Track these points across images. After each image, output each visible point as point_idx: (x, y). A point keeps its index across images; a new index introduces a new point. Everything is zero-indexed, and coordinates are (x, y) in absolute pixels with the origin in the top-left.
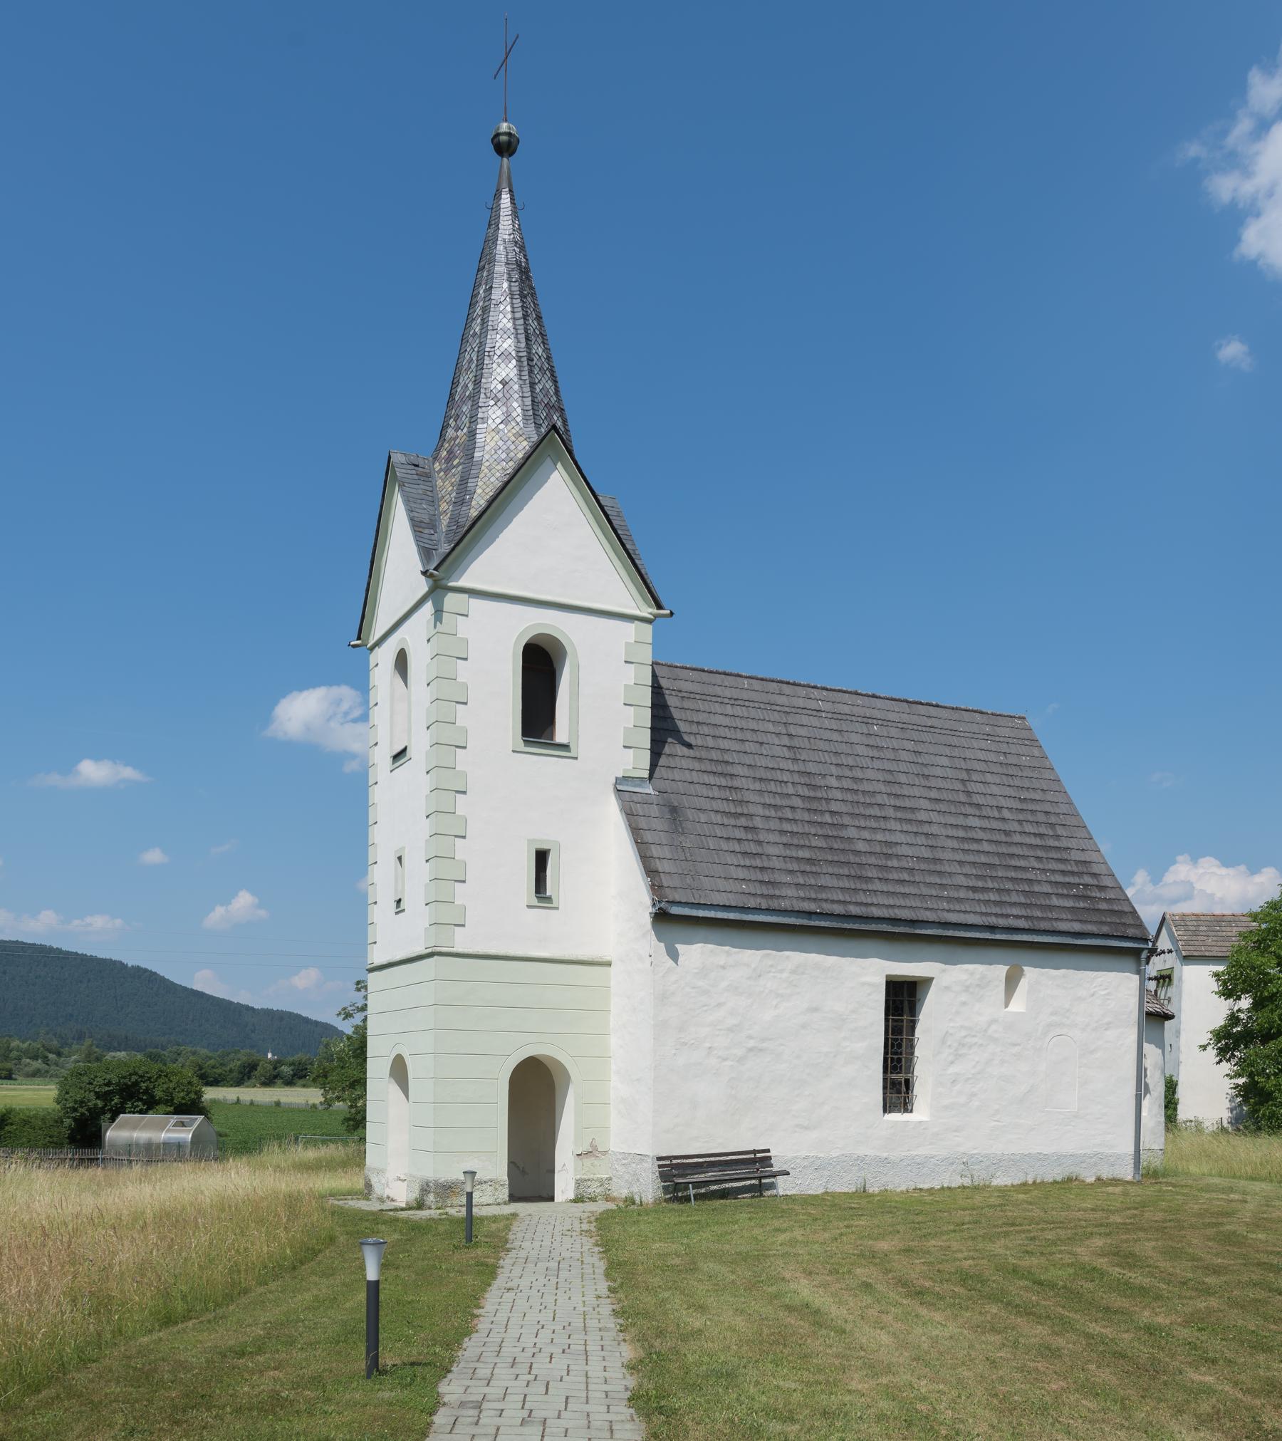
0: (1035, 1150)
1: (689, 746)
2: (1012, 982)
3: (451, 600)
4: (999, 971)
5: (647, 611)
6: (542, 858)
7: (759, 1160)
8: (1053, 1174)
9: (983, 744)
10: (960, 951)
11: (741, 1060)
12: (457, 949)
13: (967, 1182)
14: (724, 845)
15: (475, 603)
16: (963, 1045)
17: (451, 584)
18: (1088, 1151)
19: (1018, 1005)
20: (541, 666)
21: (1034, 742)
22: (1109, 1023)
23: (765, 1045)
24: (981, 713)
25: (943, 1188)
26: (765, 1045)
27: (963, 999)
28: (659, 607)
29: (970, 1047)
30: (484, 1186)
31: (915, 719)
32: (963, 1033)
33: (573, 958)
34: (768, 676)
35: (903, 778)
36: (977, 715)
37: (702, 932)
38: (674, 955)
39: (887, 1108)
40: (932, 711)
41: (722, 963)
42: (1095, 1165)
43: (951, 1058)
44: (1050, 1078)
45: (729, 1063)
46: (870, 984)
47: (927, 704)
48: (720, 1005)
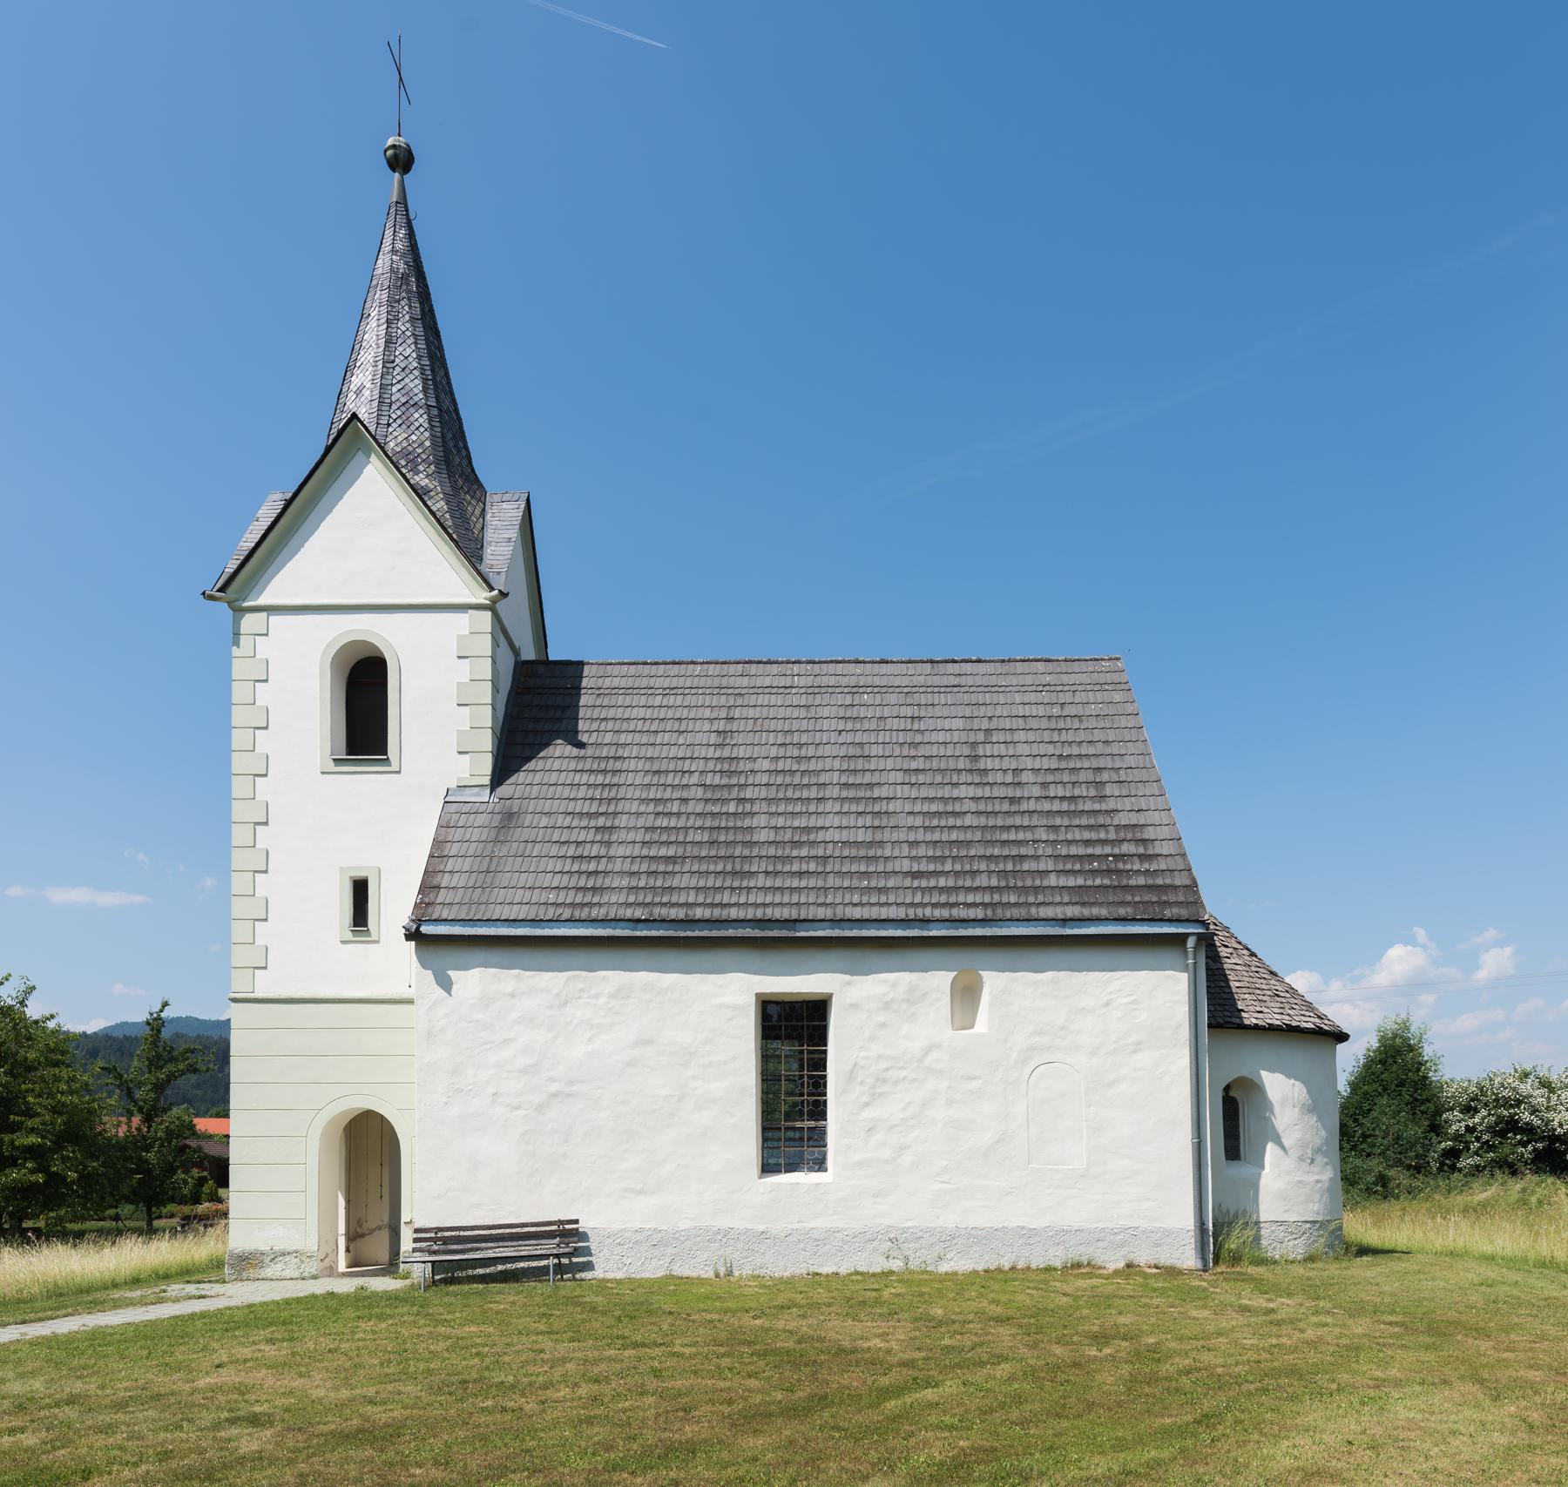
0: (1014, 1222)
1: (581, 745)
2: (966, 995)
3: (249, 622)
5: (482, 596)
6: (360, 889)
7: (568, 1233)
9: (1032, 697)
10: (873, 957)
11: (541, 1108)
12: (258, 994)
13: (896, 1265)
14: (554, 850)
16: (885, 1081)
17: (246, 604)
18: (1111, 1225)
19: (982, 1023)
22: (1139, 1043)
23: (575, 1089)
25: (1028, 1268)
26: (575, 1089)
27: (882, 1019)
28: (492, 589)
29: (897, 1083)
30: (287, 1258)
31: (937, 680)
32: (883, 1065)
35: (875, 750)
36: (1039, 664)
37: (481, 954)
38: (446, 984)
39: (767, 1168)
40: (968, 668)
41: (509, 990)
42: (1123, 1244)
43: (865, 1098)
44: (1025, 1124)
45: (522, 1112)
46: (729, 1007)
47: (963, 661)
48: (507, 1041)
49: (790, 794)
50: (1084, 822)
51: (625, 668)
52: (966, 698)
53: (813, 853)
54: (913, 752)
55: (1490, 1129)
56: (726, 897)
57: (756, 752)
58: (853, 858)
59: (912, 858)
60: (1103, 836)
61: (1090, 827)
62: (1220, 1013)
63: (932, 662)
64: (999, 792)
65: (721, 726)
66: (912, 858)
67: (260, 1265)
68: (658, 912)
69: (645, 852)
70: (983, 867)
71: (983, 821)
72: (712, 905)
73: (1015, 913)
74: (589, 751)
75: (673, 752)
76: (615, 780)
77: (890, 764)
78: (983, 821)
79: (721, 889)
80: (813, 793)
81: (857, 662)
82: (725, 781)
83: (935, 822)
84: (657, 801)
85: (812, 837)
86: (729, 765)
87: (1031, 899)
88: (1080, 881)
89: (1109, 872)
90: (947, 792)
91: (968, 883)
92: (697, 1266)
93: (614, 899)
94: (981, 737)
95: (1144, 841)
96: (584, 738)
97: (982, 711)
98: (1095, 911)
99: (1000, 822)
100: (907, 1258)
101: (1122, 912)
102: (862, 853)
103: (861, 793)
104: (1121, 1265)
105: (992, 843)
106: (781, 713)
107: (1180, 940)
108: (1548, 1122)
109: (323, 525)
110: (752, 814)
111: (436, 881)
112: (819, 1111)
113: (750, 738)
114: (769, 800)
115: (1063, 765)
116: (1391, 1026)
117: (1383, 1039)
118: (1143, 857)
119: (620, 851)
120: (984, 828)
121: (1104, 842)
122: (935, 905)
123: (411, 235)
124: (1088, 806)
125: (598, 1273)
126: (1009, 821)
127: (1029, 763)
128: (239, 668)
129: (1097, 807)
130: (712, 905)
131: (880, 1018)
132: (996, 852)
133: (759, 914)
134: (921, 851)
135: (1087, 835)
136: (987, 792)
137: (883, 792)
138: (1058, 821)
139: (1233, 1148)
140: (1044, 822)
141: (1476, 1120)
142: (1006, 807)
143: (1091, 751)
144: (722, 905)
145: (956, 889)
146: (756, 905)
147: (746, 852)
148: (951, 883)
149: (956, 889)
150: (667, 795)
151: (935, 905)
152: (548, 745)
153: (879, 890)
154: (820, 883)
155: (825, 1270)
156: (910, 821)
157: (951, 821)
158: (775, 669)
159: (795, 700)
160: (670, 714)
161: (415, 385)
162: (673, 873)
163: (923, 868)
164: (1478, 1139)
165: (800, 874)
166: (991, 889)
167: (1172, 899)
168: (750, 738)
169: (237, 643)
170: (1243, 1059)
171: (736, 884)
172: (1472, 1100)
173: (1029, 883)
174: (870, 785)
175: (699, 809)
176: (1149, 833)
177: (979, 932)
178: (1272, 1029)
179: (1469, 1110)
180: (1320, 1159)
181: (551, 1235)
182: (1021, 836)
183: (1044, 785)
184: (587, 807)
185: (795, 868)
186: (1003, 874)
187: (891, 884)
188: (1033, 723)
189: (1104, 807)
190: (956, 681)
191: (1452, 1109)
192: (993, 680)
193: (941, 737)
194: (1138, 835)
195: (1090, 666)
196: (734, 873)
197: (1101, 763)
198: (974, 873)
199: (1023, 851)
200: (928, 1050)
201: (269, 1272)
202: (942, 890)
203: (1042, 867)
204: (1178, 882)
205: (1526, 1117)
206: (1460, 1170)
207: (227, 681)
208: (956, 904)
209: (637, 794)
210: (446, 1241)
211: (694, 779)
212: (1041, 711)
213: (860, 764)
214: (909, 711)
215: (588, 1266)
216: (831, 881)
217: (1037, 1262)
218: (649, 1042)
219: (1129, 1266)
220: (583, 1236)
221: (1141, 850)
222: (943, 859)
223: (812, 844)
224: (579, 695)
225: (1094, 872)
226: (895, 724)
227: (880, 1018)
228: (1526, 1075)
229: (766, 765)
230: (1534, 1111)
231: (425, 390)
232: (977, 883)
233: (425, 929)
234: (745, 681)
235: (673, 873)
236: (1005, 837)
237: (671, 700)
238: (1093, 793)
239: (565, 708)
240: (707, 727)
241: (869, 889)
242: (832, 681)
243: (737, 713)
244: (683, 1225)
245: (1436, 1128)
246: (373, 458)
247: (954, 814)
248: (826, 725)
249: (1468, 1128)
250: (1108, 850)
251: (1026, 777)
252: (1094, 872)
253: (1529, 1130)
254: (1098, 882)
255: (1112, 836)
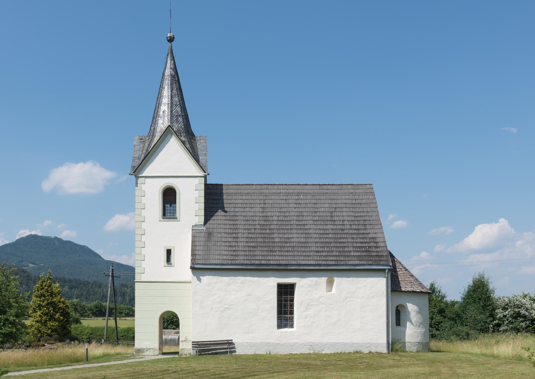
1: (226, 212)
2: (330, 283)
3: (140, 180)
4: (323, 280)
5: (202, 174)
6: (169, 252)
7: (230, 343)
8: (352, 350)
9: (347, 197)
10: (307, 273)
13: (312, 352)
14: (223, 244)
15: (147, 180)
17: (140, 176)
19: (334, 291)
20: (169, 196)
21: (373, 194)
24: (352, 185)
28: (205, 172)
29: (312, 306)
31: (321, 191)
32: (309, 301)
33: (179, 281)
34: (263, 183)
35: (305, 214)
36: (350, 186)
37: (208, 272)
38: (200, 280)
39: (280, 326)
40: (329, 187)
41: (215, 281)
42: (369, 347)
43: (304, 310)
48: (214, 295)
49: (283, 227)
50: (361, 236)
51: (234, 186)
52: (329, 197)
53: (290, 245)
54: (315, 215)
55: (511, 316)
56: (269, 258)
57: (273, 214)
58: (301, 247)
59: (316, 247)
60: (365, 241)
61: (362, 238)
62: (395, 287)
63: (319, 185)
64: (339, 227)
65: (262, 206)
66: (316, 247)
67: (144, 352)
68: (253, 262)
69: (247, 244)
70: (334, 250)
71: (334, 236)
72: (266, 260)
73: (343, 263)
74: (228, 214)
75: (250, 214)
76: (236, 223)
77: (309, 218)
78: (334, 236)
79: (268, 255)
80: (289, 227)
81: (298, 185)
82: (265, 223)
83: (322, 236)
84: (248, 229)
85: (290, 240)
86: (266, 219)
87: (347, 259)
88: (359, 254)
89: (367, 251)
90: (324, 227)
91: (331, 254)
92: (262, 351)
93: (241, 258)
94: (333, 210)
95: (376, 242)
96: (226, 209)
97: (334, 201)
98: (363, 262)
99: (339, 236)
100: (314, 350)
101: (370, 263)
102: (303, 245)
103: (302, 227)
104: (368, 352)
105: (337, 242)
106: (279, 202)
107: (384, 270)
108: (531, 314)
109: (160, 154)
110: (273, 233)
111: (195, 253)
112: (292, 313)
113: (271, 210)
114: (278, 229)
115: (356, 219)
116: (477, 276)
117: (474, 282)
118: (376, 247)
119: (240, 244)
120: (335, 238)
121: (366, 242)
122: (322, 260)
123: (174, 62)
124: (362, 232)
125: (237, 353)
126: (341, 236)
127: (346, 218)
128: (137, 193)
129: (364, 232)
130: (266, 260)
131: (307, 289)
132: (338, 245)
133: (278, 262)
134: (318, 245)
135: (362, 240)
136: (335, 227)
137: (308, 227)
138: (354, 236)
139: (398, 323)
140: (350, 236)
141: (507, 313)
142: (340, 232)
143: (363, 215)
144: (268, 260)
145: (328, 256)
146: (277, 260)
147: (273, 245)
148: (326, 254)
149: (328, 256)
150: (250, 227)
151: (322, 260)
152: (216, 212)
153: (308, 256)
154: (293, 254)
155: (293, 353)
156: (315, 236)
157: (326, 236)
158: (276, 187)
159: (282, 197)
160: (248, 202)
161: (179, 109)
162: (255, 251)
163: (319, 250)
164: (507, 320)
165: (288, 251)
166: (336, 256)
167: (382, 259)
168: (271, 210)
169: (137, 186)
170: (400, 300)
171: (272, 254)
172: (506, 305)
173: (346, 254)
174: (304, 225)
175: (259, 232)
176: (378, 240)
177: (334, 268)
178: (408, 291)
179: (505, 309)
180: (421, 326)
181: (226, 343)
182: (344, 241)
183: (351, 225)
184: (229, 231)
185: (286, 249)
186: (340, 251)
187: (311, 254)
188: (348, 206)
189: (366, 232)
190: (326, 191)
191: (499, 308)
192: (337, 191)
193: (322, 210)
194: (375, 241)
195: (364, 187)
196: (271, 251)
197: (366, 218)
198: (332, 251)
199: (345, 245)
200: (320, 298)
201: (146, 354)
202: (324, 256)
203: (350, 250)
204: (384, 254)
205: (523, 312)
206: (500, 331)
207: (134, 196)
208: (328, 260)
209: (242, 227)
210: (199, 344)
211: (257, 222)
212: (350, 201)
213: (301, 218)
214: (313, 201)
215: (235, 351)
216: (296, 253)
217: (347, 351)
218: (250, 295)
219: (370, 352)
220: (234, 344)
221: (375, 245)
222: (324, 247)
223: (290, 242)
224: (223, 195)
225: (363, 251)
226: (310, 205)
227: (307, 289)
228: (525, 296)
229: (276, 218)
230: (527, 310)
231: (181, 111)
232: (333, 254)
233: (196, 266)
234: (267, 191)
235: (255, 251)
236: (340, 241)
237: (248, 197)
238: (363, 228)
239: (219, 200)
240: (258, 206)
241: (305, 256)
242: (292, 191)
243: (266, 202)
244: (258, 341)
245: (492, 316)
246: (173, 136)
247: (327, 234)
248: (291, 205)
249: (503, 315)
250: (367, 245)
251: (346, 223)
252: (363, 251)
253: (524, 317)
254: (364, 254)
255: (368, 241)
